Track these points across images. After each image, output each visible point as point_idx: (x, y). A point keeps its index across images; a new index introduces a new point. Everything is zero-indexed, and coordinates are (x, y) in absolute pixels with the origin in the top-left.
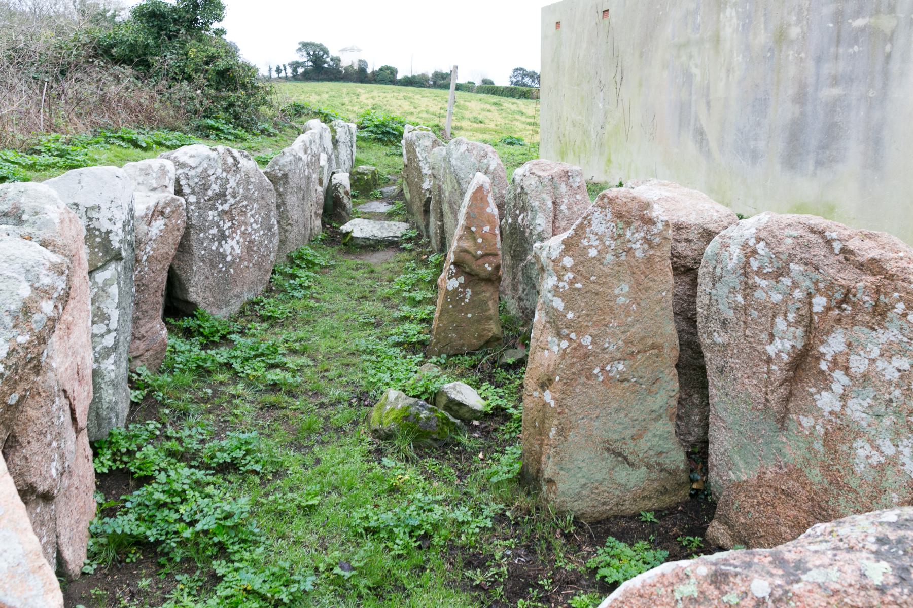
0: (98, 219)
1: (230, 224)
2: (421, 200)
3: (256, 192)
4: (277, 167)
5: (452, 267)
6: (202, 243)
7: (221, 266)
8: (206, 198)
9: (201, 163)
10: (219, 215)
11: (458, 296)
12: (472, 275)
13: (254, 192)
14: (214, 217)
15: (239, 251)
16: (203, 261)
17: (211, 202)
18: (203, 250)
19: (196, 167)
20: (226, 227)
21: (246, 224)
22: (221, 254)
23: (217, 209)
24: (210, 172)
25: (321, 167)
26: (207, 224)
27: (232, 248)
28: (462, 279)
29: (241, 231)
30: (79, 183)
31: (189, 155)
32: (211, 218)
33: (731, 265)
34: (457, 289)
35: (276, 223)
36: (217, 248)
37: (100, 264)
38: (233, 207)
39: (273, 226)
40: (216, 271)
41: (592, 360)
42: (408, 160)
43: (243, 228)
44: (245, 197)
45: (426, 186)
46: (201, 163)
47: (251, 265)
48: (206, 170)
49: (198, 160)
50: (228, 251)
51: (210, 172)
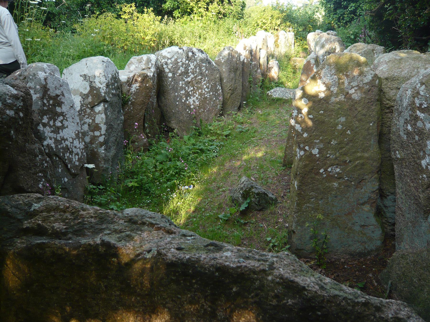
0: (95, 82)
8: (178, 74)
10: (185, 84)
14: (182, 84)
15: (198, 103)
17: (181, 77)
29: (199, 92)
30: (86, 65)
32: (181, 85)
33: (405, 104)
37: (96, 104)
41: (318, 164)
43: (200, 91)
50: (192, 103)
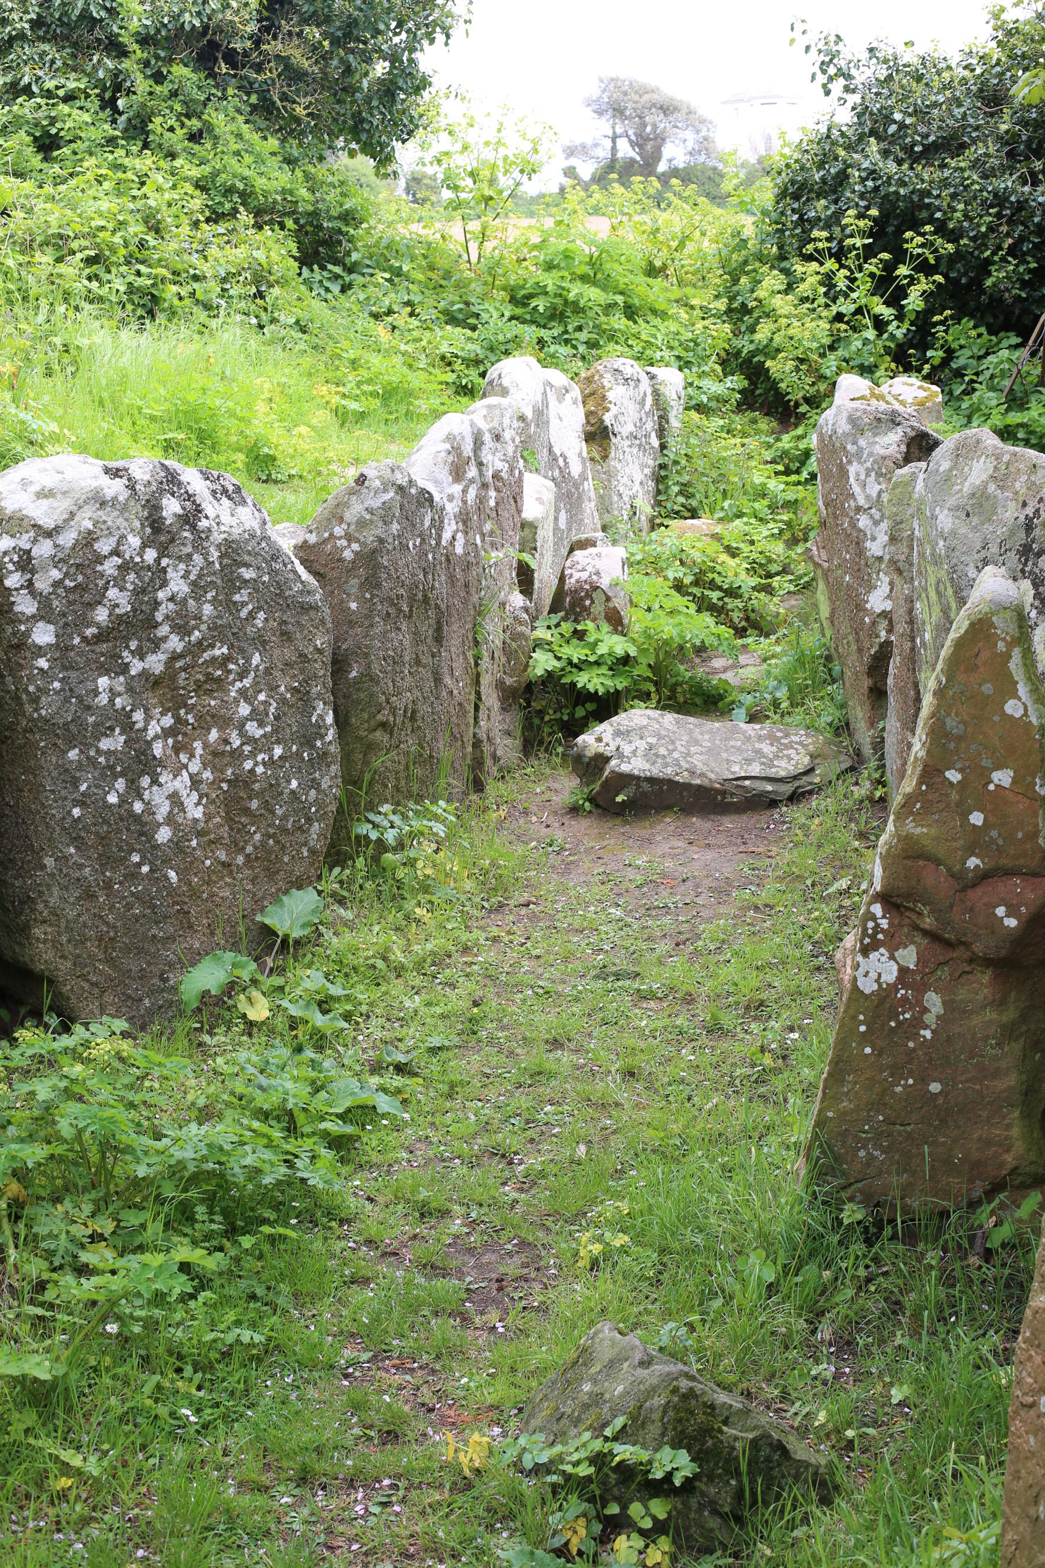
1: (168, 721)
2: (860, 650)
3: (261, 615)
4: (338, 531)
5: (877, 909)
6: (75, 783)
7: (136, 858)
8: (90, 632)
9: (72, 515)
11: (895, 1016)
12: (949, 944)
13: (252, 616)
14: (113, 694)
15: (198, 813)
16: (77, 840)
17: (104, 647)
18: (76, 803)
19: (57, 530)
20: (154, 729)
21: (224, 722)
22: (137, 818)
23: (125, 668)
24: (104, 547)
25: (524, 525)
26: (91, 720)
27: (174, 798)
28: (909, 956)
29: (206, 745)
31: (37, 488)
32: (103, 699)
34: (893, 988)
35: (330, 719)
36: (123, 801)
38: (179, 664)
39: (319, 731)
40: (118, 877)
42: (827, 505)
43: (214, 735)
44: (217, 632)
45: (878, 601)
46: (72, 515)
47: (240, 860)
48: (88, 539)
49: (64, 505)
50: (163, 810)
51: (104, 547)
